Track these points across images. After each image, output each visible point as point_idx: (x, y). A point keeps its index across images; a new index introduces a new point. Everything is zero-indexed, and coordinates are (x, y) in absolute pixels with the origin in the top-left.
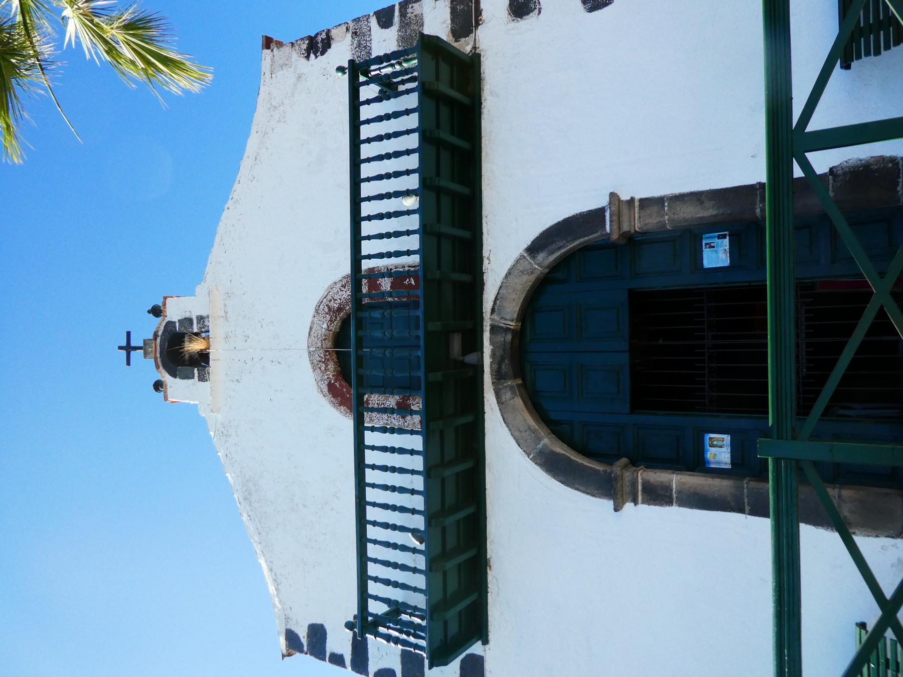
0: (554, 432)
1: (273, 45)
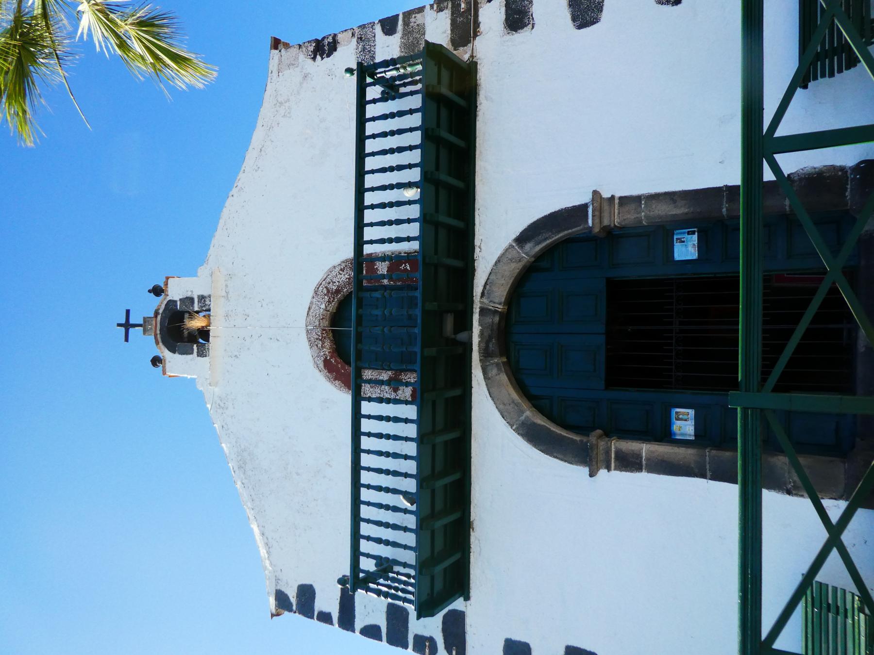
0: (535, 406)
1: (280, 46)
